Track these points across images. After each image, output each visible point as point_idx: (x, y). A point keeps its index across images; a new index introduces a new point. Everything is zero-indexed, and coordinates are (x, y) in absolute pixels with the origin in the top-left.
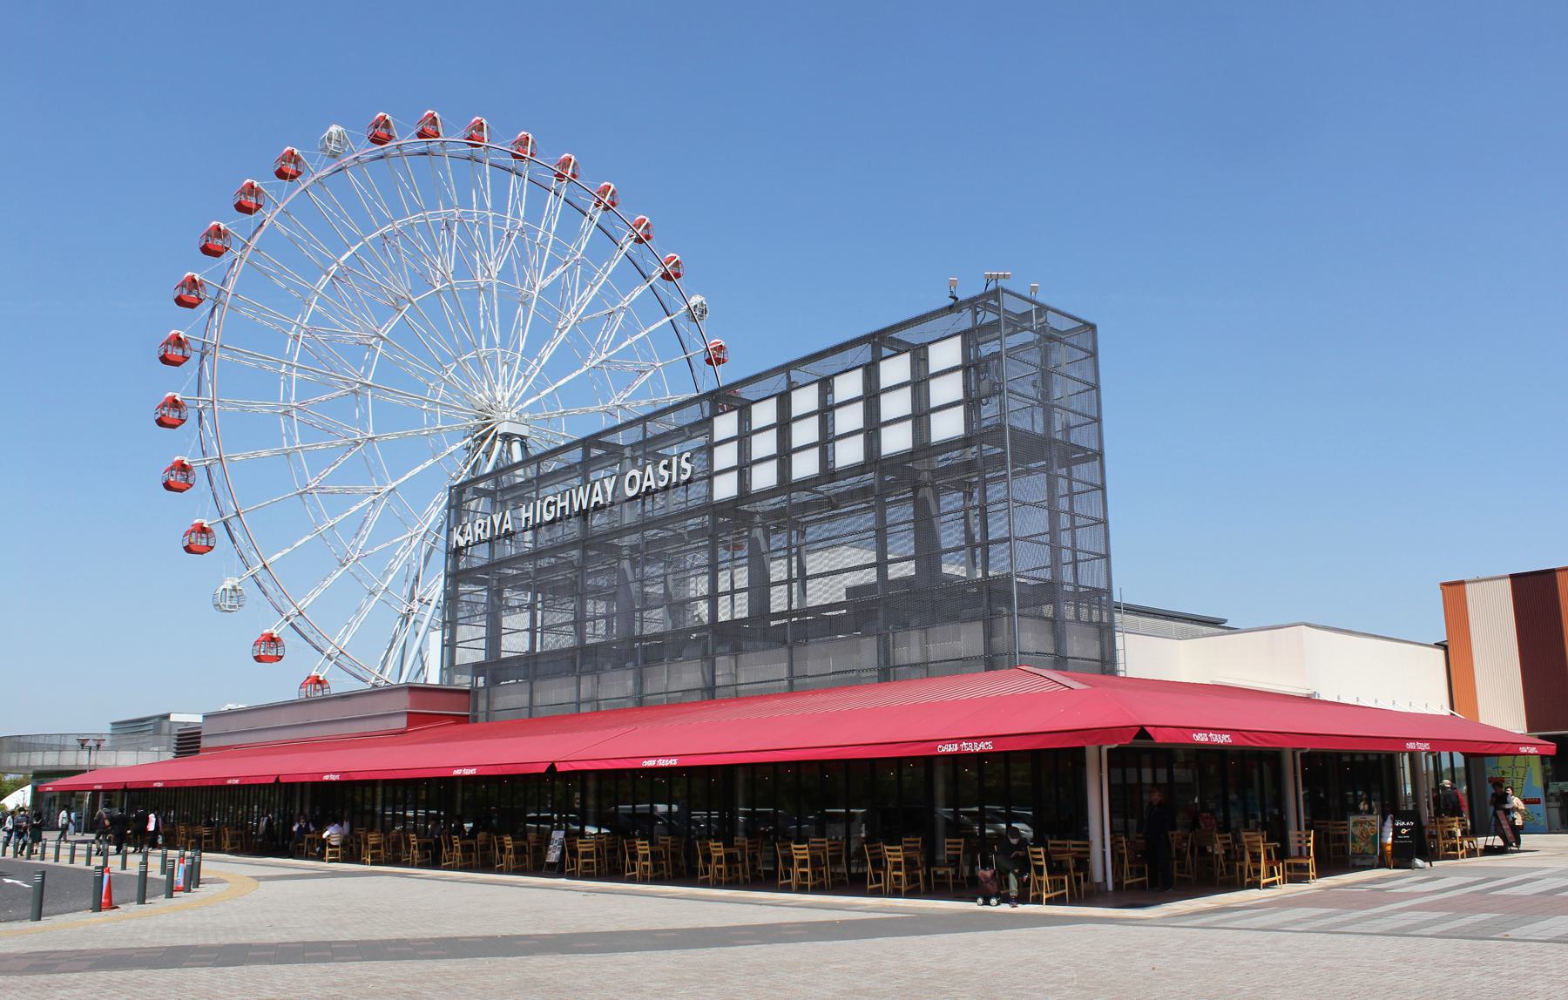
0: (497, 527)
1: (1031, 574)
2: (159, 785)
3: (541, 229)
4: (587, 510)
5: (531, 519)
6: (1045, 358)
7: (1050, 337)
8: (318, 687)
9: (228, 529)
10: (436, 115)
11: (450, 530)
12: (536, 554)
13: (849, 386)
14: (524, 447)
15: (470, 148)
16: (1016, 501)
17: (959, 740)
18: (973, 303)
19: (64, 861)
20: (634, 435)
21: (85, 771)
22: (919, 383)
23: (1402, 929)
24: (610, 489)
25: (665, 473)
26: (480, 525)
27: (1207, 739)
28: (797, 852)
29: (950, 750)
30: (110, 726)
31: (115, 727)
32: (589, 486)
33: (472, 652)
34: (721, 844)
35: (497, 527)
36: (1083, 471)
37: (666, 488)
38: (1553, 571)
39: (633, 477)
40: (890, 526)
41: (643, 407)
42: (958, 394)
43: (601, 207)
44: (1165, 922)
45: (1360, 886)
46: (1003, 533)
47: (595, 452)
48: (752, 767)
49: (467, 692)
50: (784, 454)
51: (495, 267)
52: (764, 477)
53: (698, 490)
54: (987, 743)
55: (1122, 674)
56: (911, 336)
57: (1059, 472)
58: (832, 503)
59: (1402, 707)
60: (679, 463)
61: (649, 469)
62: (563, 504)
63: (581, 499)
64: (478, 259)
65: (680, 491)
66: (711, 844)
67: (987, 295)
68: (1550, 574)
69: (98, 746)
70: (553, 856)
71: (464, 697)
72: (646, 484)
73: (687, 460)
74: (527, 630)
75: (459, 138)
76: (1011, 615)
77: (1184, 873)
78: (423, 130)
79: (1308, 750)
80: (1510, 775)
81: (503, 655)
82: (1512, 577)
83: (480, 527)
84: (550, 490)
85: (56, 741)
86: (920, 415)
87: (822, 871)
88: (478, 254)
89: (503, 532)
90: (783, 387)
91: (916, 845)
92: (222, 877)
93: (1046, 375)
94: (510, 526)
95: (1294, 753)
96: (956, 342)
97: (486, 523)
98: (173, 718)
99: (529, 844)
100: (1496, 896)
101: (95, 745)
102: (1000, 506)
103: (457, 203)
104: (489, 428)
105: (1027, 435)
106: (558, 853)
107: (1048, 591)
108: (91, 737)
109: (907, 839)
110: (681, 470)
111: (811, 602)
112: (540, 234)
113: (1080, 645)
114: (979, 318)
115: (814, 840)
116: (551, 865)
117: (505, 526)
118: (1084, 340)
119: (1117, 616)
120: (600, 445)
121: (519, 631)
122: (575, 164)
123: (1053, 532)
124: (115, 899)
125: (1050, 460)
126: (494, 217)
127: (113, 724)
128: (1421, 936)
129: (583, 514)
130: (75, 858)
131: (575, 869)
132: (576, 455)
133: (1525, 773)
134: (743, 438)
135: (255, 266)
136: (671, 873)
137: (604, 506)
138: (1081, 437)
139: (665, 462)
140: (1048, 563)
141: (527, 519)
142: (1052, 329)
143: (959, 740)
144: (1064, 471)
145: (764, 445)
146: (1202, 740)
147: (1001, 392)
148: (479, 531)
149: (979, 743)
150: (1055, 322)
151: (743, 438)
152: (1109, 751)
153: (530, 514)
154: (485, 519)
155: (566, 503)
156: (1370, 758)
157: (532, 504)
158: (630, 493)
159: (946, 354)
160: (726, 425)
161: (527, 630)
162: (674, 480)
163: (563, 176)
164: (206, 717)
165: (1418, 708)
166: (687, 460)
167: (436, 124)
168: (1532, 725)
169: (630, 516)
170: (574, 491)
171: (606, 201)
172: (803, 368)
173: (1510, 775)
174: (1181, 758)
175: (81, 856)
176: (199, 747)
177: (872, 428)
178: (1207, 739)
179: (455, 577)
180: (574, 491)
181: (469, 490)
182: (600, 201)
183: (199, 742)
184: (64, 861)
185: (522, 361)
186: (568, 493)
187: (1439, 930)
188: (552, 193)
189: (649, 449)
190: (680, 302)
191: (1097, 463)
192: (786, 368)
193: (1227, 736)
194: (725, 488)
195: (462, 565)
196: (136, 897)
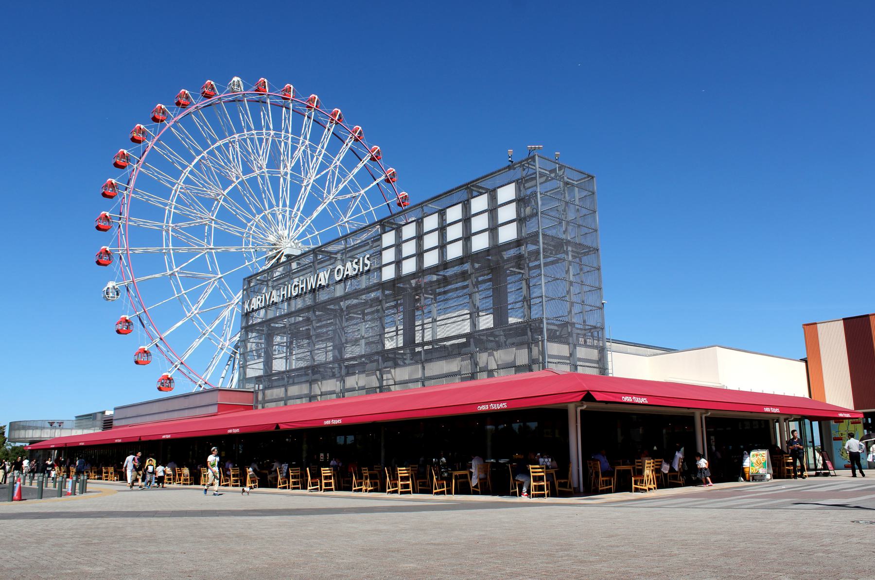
0: (268, 300)
1: (561, 319)
2: (82, 444)
5: (285, 295)
11: (243, 303)
12: (289, 315)
13: (454, 213)
17: (488, 403)
20: (340, 246)
22: (492, 210)
25: (356, 267)
26: (259, 299)
27: (631, 400)
29: (484, 409)
31: (77, 419)
32: (316, 275)
33: (256, 369)
34: (367, 468)
35: (268, 300)
38: (868, 316)
39: (339, 269)
42: (513, 216)
54: (504, 404)
55: (610, 375)
60: (363, 261)
62: (302, 286)
63: (312, 282)
68: (866, 317)
71: (252, 393)
72: (346, 273)
73: (368, 259)
76: (543, 341)
77: (643, 486)
81: (273, 372)
82: (844, 319)
83: (259, 301)
84: (296, 280)
85: (39, 425)
86: (493, 229)
90: (420, 216)
96: (512, 186)
97: (262, 299)
108: (56, 422)
110: (365, 265)
119: (608, 344)
126: (292, 137)
127: (76, 417)
129: (313, 291)
134: (398, 246)
137: (324, 286)
139: (356, 260)
141: (283, 295)
149: (499, 404)
151: (398, 246)
152: (581, 411)
153: (285, 292)
154: (262, 296)
155: (304, 285)
157: (286, 287)
158: (338, 279)
159: (507, 193)
160: (389, 238)
162: (361, 270)
164: (115, 409)
166: (368, 258)
169: (339, 291)
176: (112, 425)
178: (631, 400)
179: (247, 329)
180: (308, 279)
182: (332, 120)
189: (349, 254)
192: (421, 205)
194: (388, 273)
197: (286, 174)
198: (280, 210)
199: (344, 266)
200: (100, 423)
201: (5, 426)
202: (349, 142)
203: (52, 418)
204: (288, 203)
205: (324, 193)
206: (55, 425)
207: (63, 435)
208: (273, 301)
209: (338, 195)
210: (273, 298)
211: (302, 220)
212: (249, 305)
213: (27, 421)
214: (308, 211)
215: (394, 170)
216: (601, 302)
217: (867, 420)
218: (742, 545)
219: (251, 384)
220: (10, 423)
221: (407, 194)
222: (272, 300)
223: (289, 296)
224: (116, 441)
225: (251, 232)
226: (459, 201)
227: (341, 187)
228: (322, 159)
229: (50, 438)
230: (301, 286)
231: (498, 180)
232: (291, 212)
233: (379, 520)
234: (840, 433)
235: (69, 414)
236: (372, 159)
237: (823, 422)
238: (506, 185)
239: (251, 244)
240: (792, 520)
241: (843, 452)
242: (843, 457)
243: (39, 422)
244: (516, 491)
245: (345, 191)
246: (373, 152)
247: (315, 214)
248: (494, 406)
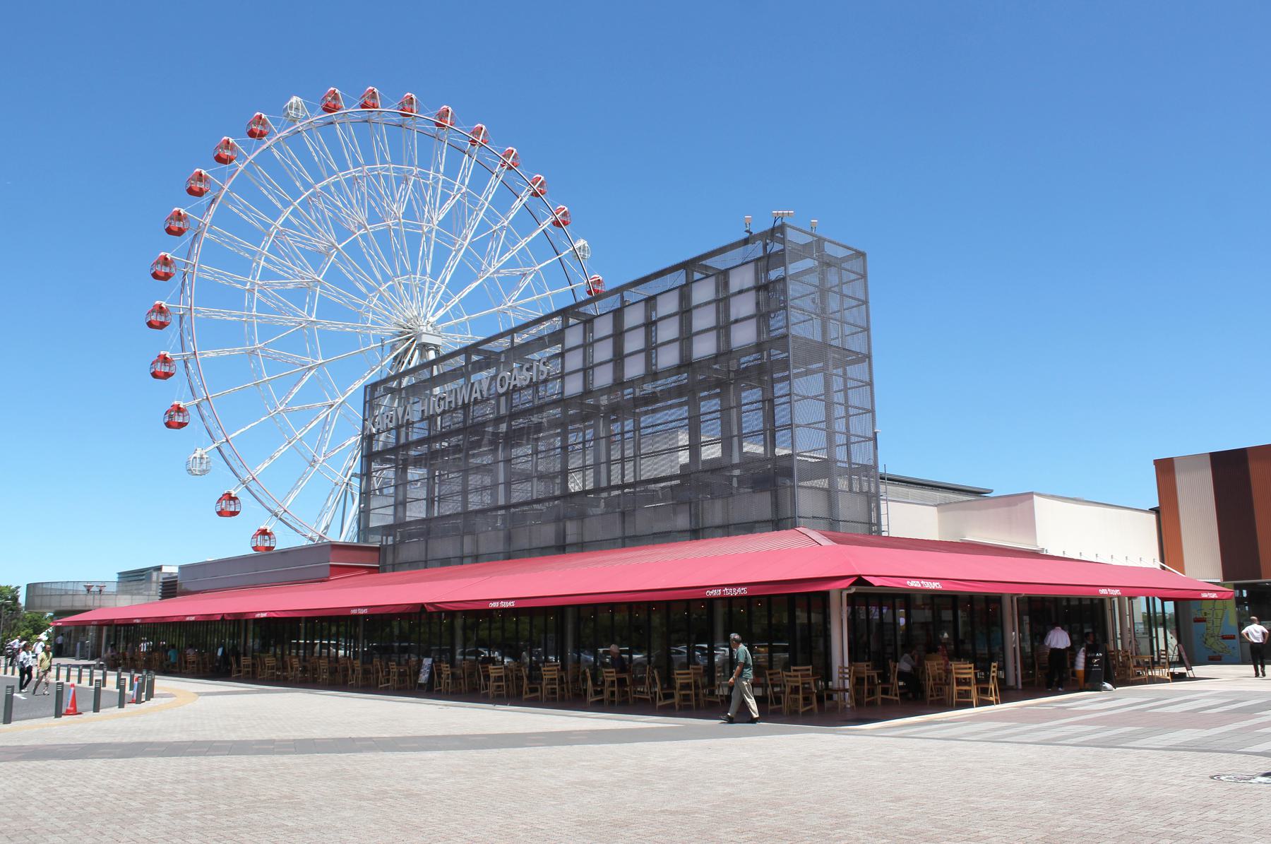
0: (400, 417)
3: (457, 183)
4: (469, 403)
5: (426, 411)
6: (822, 280)
7: (827, 263)
10: (376, 90)
14: (437, 352)
15: (402, 118)
16: (797, 395)
18: (763, 235)
19: (74, 680)
20: (504, 343)
21: (91, 610)
22: (722, 301)
23: (1054, 739)
26: (387, 416)
28: (607, 674)
30: (117, 576)
31: (121, 576)
35: (400, 417)
36: (855, 371)
39: (503, 377)
40: (703, 414)
41: (514, 320)
43: (506, 167)
44: (872, 733)
45: (1050, 705)
46: (785, 420)
47: (475, 358)
48: (578, 608)
49: (378, 549)
50: (619, 358)
51: (399, 209)
52: (603, 377)
53: (555, 387)
56: (717, 263)
57: (835, 371)
58: (651, 399)
59: (1119, 561)
60: (538, 366)
64: (426, 210)
66: (490, 667)
67: (773, 230)
69: (100, 591)
70: (423, 678)
71: (376, 554)
74: (425, 499)
75: (395, 109)
78: (365, 102)
79: (1023, 595)
80: (1210, 616)
86: (723, 328)
87: (781, 697)
88: (427, 207)
89: (405, 421)
90: (618, 305)
91: (807, 672)
92: (173, 693)
93: (823, 291)
95: (1012, 597)
98: (165, 569)
99: (410, 668)
100: (1164, 714)
101: (98, 590)
102: (783, 400)
103: (416, 163)
104: (411, 341)
105: (807, 342)
106: (427, 676)
107: (825, 468)
108: (95, 584)
109: (795, 668)
111: (628, 480)
112: (456, 187)
113: (849, 508)
114: (769, 248)
115: (678, 672)
116: (421, 686)
118: (856, 265)
119: (882, 488)
120: (478, 352)
121: (418, 500)
122: (485, 132)
123: (829, 420)
124: (79, 708)
125: (826, 365)
127: (119, 573)
128: (1134, 748)
129: (465, 406)
130: (71, 677)
131: (539, 694)
132: (460, 361)
133: (1223, 615)
136: (467, 689)
138: (856, 344)
139: (527, 365)
140: (824, 445)
142: (829, 255)
143: (723, 586)
144: (840, 371)
145: (604, 352)
146: (915, 585)
147: (785, 308)
149: (737, 589)
150: (830, 249)
155: (453, 399)
156: (1072, 603)
161: (425, 499)
163: (476, 142)
164: (181, 568)
165: (1133, 562)
167: (412, 103)
168: (1228, 574)
171: (509, 162)
172: (633, 290)
173: (1210, 616)
174: (919, 602)
175: (86, 676)
176: (176, 592)
177: (686, 337)
181: (381, 389)
182: (505, 162)
183: (176, 588)
184: (74, 680)
185: (445, 292)
187: (1082, 740)
188: (467, 156)
190: (566, 243)
191: (866, 364)
193: (938, 583)
194: (574, 386)
196: (92, 707)
197: (430, 231)
198: (418, 279)
200: (155, 589)
201: (18, 587)
202: (524, 196)
204: (429, 270)
205: (482, 264)
208: (408, 420)
209: (503, 267)
210: (408, 414)
211: (446, 298)
213: (62, 582)
214: (456, 286)
215: (566, 209)
216: (873, 429)
217: (1241, 593)
218: (1071, 820)
220: (28, 585)
221: (601, 278)
222: (406, 417)
224: (188, 619)
225: (372, 305)
226: (749, 259)
227: (507, 256)
228: (484, 215)
232: (432, 284)
233: (584, 761)
234: (1203, 612)
235: (107, 574)
236: (556, 223)
237: (1179, 603)
239: (370, 321)
240: (1134, 771)
241: (1206, 639)
242: (1206, 645)
243: (69, 584)
244: (304, 194)
245: (511, 263)
246: (534, 184)
247: (467, 291)
248: (729, 591)
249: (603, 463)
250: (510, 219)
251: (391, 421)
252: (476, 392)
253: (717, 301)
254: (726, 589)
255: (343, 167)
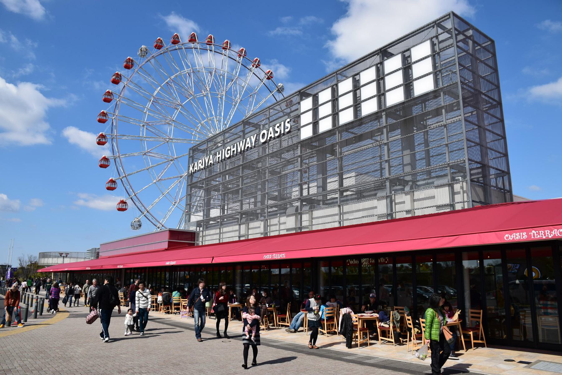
4: (244, 151)
8: (124, 205)
9: (115, 162)
13: (325, 96)
24: (253, 140)
26: (200, 162)
33: (197, 217)
37: (278, 137)
54: (283, 254)
61: (271, 129)
63: (241, 146)
65: (286, 137)
69: (67, 256)
72: (269, 136)
94: (212, 162)
97: (202, 162)
117: (210, 162)
135: (149, 130)
139: (278, 125)
141: (219, 158)
148: (200, 165)
151: (315, 110)
155: (235, 149)
160: (307, 104)
162: (282, 132)
163: (241, 55)
166: (288, 122)
170: (238, 143)
180: (238, 143)
186: (236, 144)
194: (306, 133)
195: (195, 180)
199: (268, 130)
203: (62, 251)
206: (64, 255)
207: (72, 262)
212: (193, 168)
219: (194, 227)
223: (223, 158)
226: (372, 64)
229: (57, 263)
230: (232, 150)
231: (321, 87)
238: (419, 44)
248: (275, 256)
249: (259, 202)
250: (222, 115)
251: (202, 165)
252: (248, 144)
253: (359, 88)
254: (274, 255)
255: (182, 68)
